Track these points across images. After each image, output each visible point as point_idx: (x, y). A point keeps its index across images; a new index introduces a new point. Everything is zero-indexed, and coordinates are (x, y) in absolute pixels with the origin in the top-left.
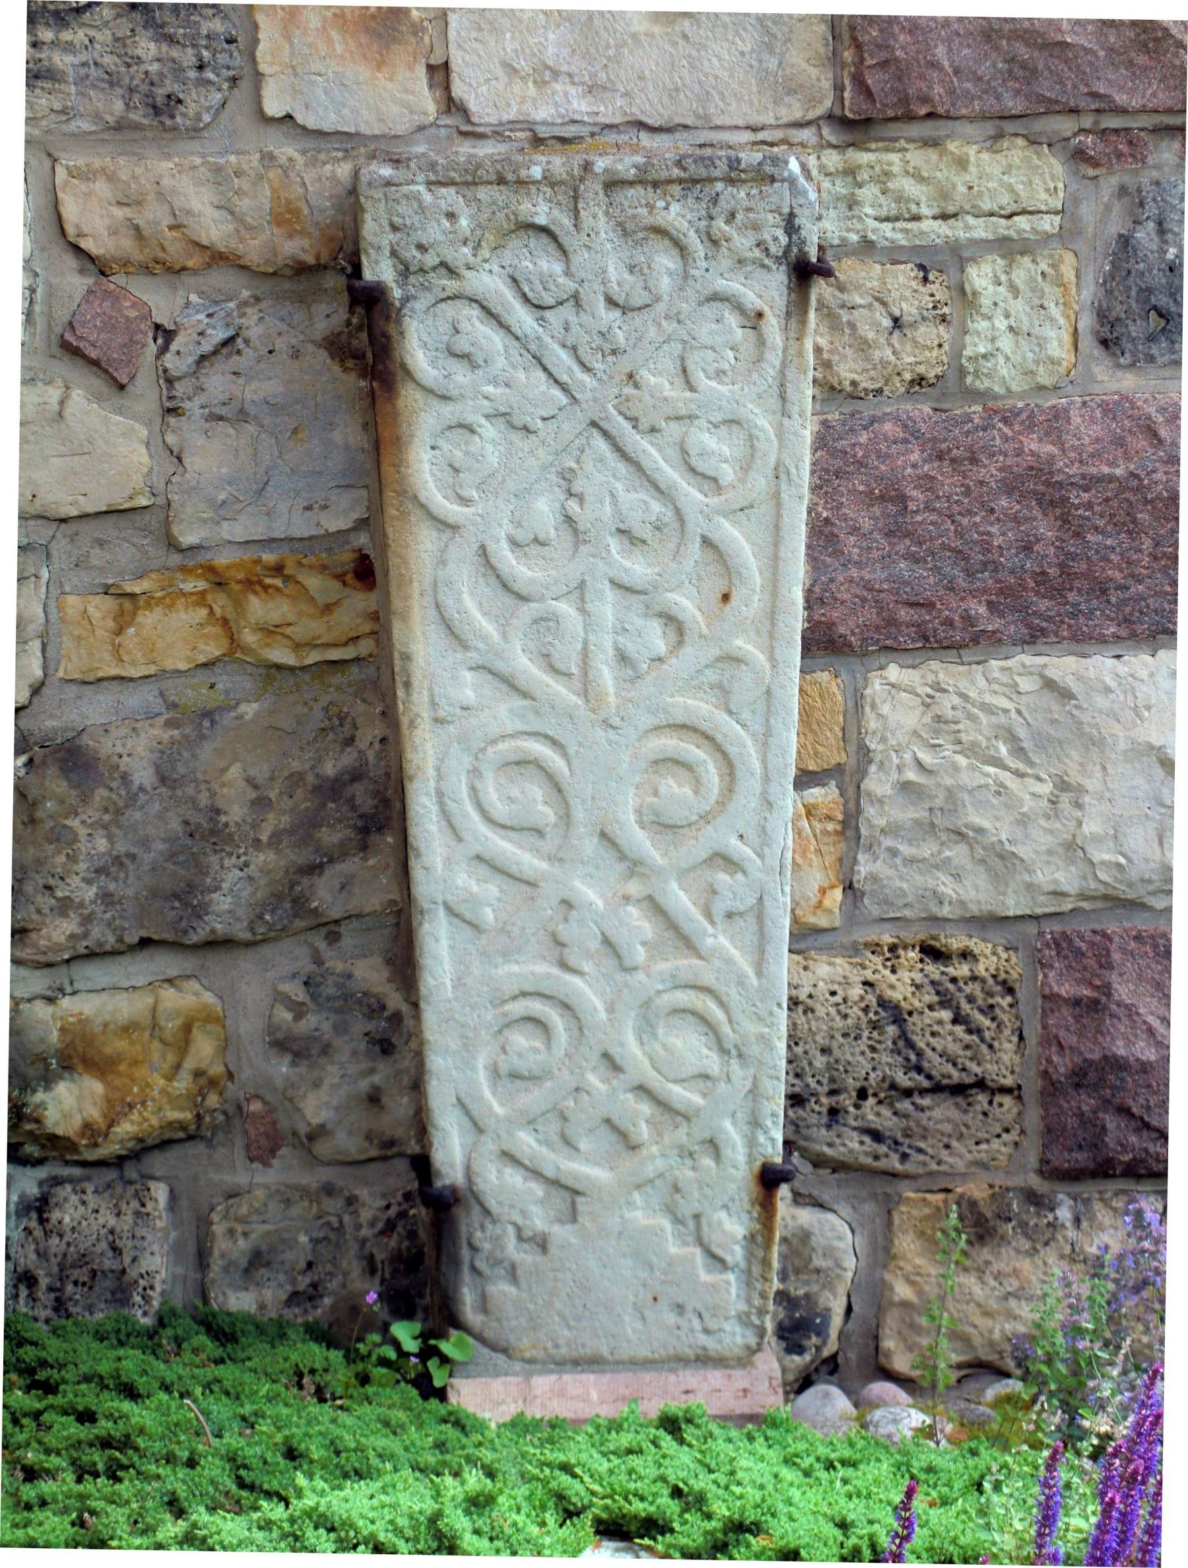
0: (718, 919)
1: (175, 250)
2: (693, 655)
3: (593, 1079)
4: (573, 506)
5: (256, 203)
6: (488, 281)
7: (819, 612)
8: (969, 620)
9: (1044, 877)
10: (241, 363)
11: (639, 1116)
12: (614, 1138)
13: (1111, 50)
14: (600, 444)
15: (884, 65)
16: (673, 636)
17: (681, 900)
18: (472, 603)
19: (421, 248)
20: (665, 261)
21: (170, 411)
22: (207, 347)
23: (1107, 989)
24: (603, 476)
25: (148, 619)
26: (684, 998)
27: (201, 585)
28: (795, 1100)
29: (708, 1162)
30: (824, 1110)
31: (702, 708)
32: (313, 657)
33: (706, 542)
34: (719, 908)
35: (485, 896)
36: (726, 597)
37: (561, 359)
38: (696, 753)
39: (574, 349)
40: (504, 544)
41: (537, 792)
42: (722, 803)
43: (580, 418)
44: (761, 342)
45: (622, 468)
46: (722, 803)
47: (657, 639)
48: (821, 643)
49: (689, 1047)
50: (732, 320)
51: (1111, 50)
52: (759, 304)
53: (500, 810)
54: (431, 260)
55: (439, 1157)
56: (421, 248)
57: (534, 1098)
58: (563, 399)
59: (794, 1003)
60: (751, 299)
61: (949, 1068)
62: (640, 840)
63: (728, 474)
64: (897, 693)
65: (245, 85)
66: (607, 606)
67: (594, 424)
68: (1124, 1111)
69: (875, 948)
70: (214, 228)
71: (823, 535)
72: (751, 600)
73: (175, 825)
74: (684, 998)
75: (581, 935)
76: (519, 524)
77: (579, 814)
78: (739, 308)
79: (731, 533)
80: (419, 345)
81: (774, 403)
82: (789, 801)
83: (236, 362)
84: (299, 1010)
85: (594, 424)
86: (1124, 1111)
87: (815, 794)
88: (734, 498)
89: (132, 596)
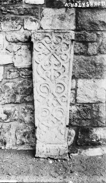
0: (63, 102)
1: (16, 40)
2: (61, 76)
3: (50, 117)
4: (50, 62)
5: (23, 36)
6: (43, 41)
7: (73, 74)
8: (87, 75)
9: (93, 99)
10: (21, 50)
11: (55, 120)
12: (52, 122)
13: (101, 25)
14: (53, 56)
15: (80, 25)
16: (59, 74)
17: (59, 100)
18: (40, 71)
19: (37, 38)
20: (60, 40)
21: (14, 55)
22: (18, 49)
23: (99, 110)
24: (53, 59)
25: (12, 73)
26: (60, 109)
27: (16, 70)
28: (70, 120)
29: (61, 125)
30: (45, 15)
31: (62, 82)
32: (27, 77)
33: (63, 66)
34: (63, 101)
35: (41, 99)
36: (65, 71)
37: (50, 49)
38: (61, 86)
39: (51, 47)
40: (44, 66)
41: (46, 89)
42: (63, 91)
43: (50, 54)
44: (68, 47)
45: (55, 58)
46: (63, 91)
47: (58, 75)
48: (73, 77)
49: (60, 114)
50: (66, 45)
51: (101, 25)
52: (68, 44)
53: (41, 90)
54: (37, 39)
55: (36, 124)
56: (37, 38)
57: (46, 119)
58: (50, 52)
59: (70, 110)
60: (68, 43)
61: (49, 146)
62: (56, 94)
63: (65, 60)
64: (81, 82)
65: (23, 26)
66: (53, 71)
67: (52, 54)
68: (100, 121)
69: (78, 106)
70: (19, 39)
71: (74, 67)
72: (67, 71)
73: (14, 92)
74: (60, 109)
75: (50, 104)
76: (45, 63)
77: (65, 111)
78: (66, 44)
79: (65, 65)
80: (35, 46)
81: (70, 53)
82: (70, 91)
83: (21, 50)
84: (24, 109)
85: (52, 54)
86: (100, 121)
87: (72, 91)
88: (65, 62)
89: (11, 71)
